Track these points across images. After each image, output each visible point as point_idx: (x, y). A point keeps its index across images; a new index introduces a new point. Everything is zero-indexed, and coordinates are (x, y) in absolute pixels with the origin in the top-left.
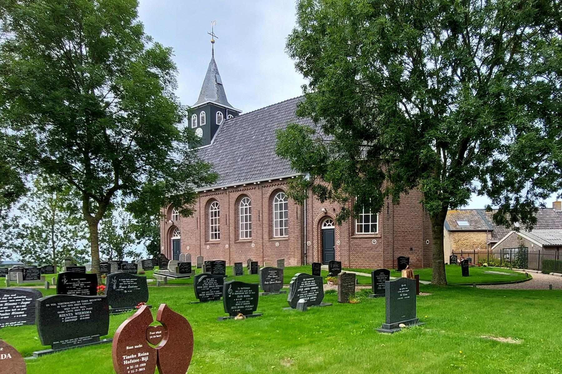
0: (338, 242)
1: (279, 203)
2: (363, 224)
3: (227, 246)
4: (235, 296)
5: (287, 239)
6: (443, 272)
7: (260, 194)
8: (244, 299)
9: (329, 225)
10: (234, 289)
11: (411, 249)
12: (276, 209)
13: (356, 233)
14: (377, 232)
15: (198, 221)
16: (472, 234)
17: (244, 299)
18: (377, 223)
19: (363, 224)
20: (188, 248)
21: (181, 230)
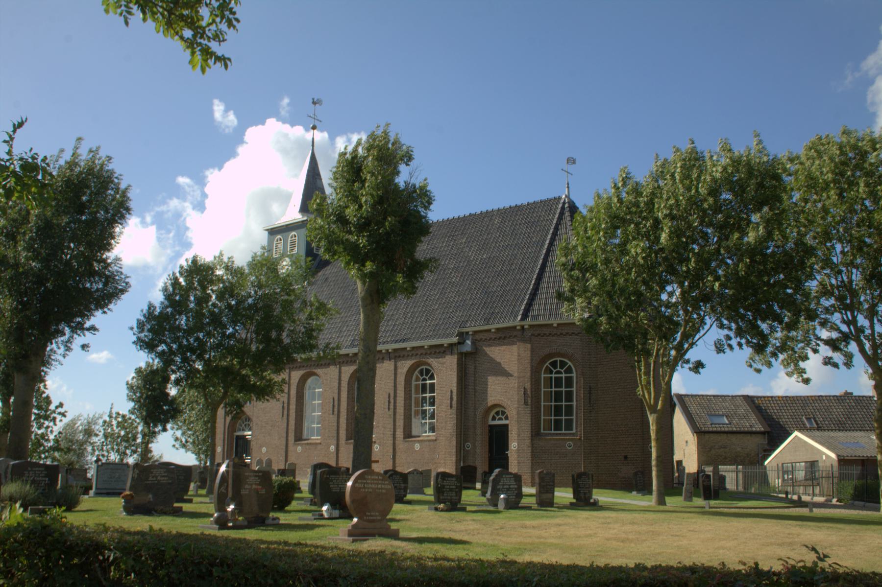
0: (513, 445)
1: (421, 383)
2: (553, 404)
3: (333, 448)
4: (444, 486)
5: (434, 438)
6: (323, 363)
7: (392, 368)
8: (451, 490)
9: (500, 419)
10: (443, 479)
11: (626, 457)
12: (417, 393)
13: (542, 431)
14: (574, 431)
15: (286, 408)
16: (734, 439)
17: (451, 490)
18: (574, 417)
19: (553, 404)
20: (264, 449)
21: (253, 425)
